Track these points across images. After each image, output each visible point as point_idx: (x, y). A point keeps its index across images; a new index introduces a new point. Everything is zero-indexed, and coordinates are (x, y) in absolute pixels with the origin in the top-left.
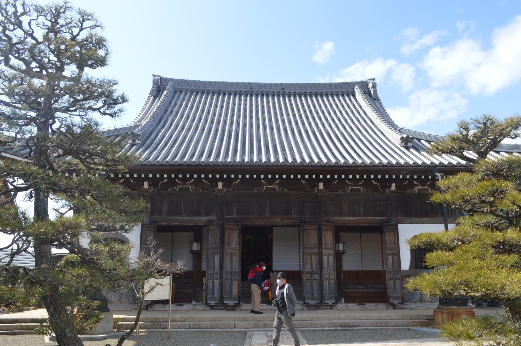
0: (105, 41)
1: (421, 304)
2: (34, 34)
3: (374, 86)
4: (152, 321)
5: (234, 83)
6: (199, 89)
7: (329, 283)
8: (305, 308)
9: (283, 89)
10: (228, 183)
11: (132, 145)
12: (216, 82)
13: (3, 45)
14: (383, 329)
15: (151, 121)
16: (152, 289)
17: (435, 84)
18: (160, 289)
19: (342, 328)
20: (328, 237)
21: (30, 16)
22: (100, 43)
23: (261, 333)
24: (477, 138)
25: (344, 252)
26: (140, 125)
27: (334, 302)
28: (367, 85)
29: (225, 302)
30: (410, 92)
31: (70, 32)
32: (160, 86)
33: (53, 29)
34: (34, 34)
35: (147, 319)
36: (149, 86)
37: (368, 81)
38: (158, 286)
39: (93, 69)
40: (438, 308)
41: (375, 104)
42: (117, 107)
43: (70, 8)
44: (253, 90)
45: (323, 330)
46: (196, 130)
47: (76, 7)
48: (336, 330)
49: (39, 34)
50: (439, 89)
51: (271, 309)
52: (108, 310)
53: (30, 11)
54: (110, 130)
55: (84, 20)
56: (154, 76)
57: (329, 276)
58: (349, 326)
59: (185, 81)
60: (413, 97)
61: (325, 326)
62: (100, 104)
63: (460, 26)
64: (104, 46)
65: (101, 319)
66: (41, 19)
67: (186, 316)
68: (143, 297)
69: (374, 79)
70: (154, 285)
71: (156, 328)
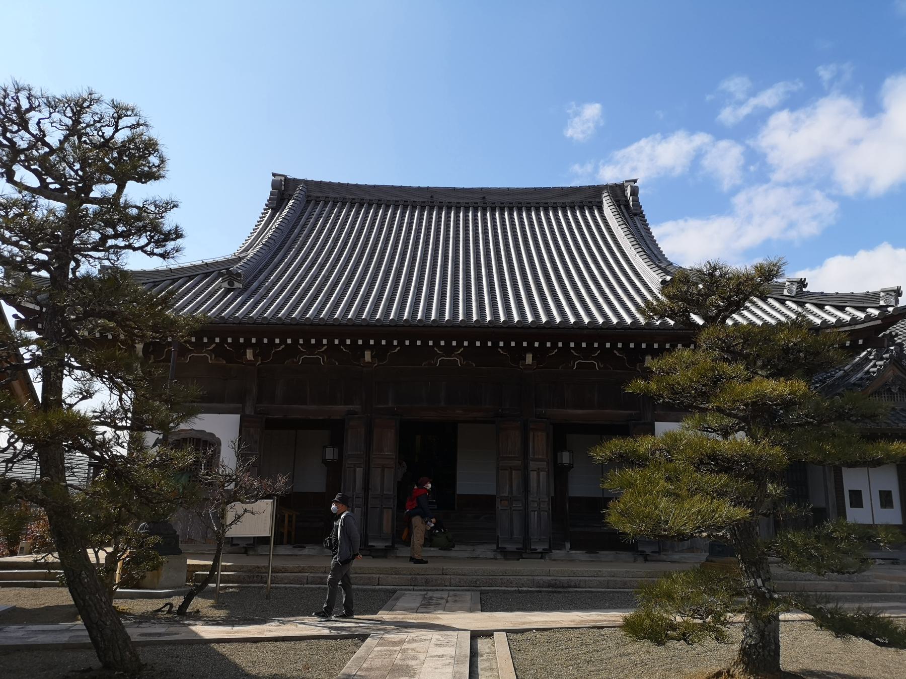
0: (157, 145)
1: (691, 555)
2: (46, 139)
3: (635, 192)
4: (250, 571)
5: (405, 187)
6: (348, 197)
7: (539, 517)
8: (499, 556)
9: (484, 198)
10: (378, 351)
11: (228, 291)
12: (374, 186)
13: (2, 153)
14: (617, 592)
15: (263, 251)
16: (238, 518)
17: (778, 176)
18: (256, 519)
19: (550, 589)
20: (539, 443)
21: (40, 111)
22: (151, 146)
23: (417, 593)
24: (702, 296)
25: (571, 466)
26: (243, 258)
27: (547, 547)
28: (625, 191)
29: (370, 544)
30: (735, 191)
31: (100, 133)
32: (283, 190)
33: (74, 130)
34: (46, 139)
35: (242, 567)
36: (265, 193)
37: (626, 184)
38: (246, 514)
39: (143, 183)
40: (707, 560)
41: (634, 223)
42: (170, 245)
43: (98, 101)
44: (435, 200)
45: (519, 592)
46: (334, 266)
47: (107, 98)
48: (541, 592)
49: (54, 137)
50: (786, 185)
51: (445, 557)
52: (179, 552)
53: (39, 105)
54: (195, 266)
55: (120, 117)
56: (274, 175)
57: (539, 505)
58: (563, 587)
59: (325, 183)
60: (740, 199)
61: (523, 586)
62: (143, 241)
63: (825, 74)
64: (156, 150)
65: (162, 563)
66: (56, 116)
67: (303, 564)
68: (224, 532)
69: (635, 181)
70: (241, 512)
71: (254, 583)
